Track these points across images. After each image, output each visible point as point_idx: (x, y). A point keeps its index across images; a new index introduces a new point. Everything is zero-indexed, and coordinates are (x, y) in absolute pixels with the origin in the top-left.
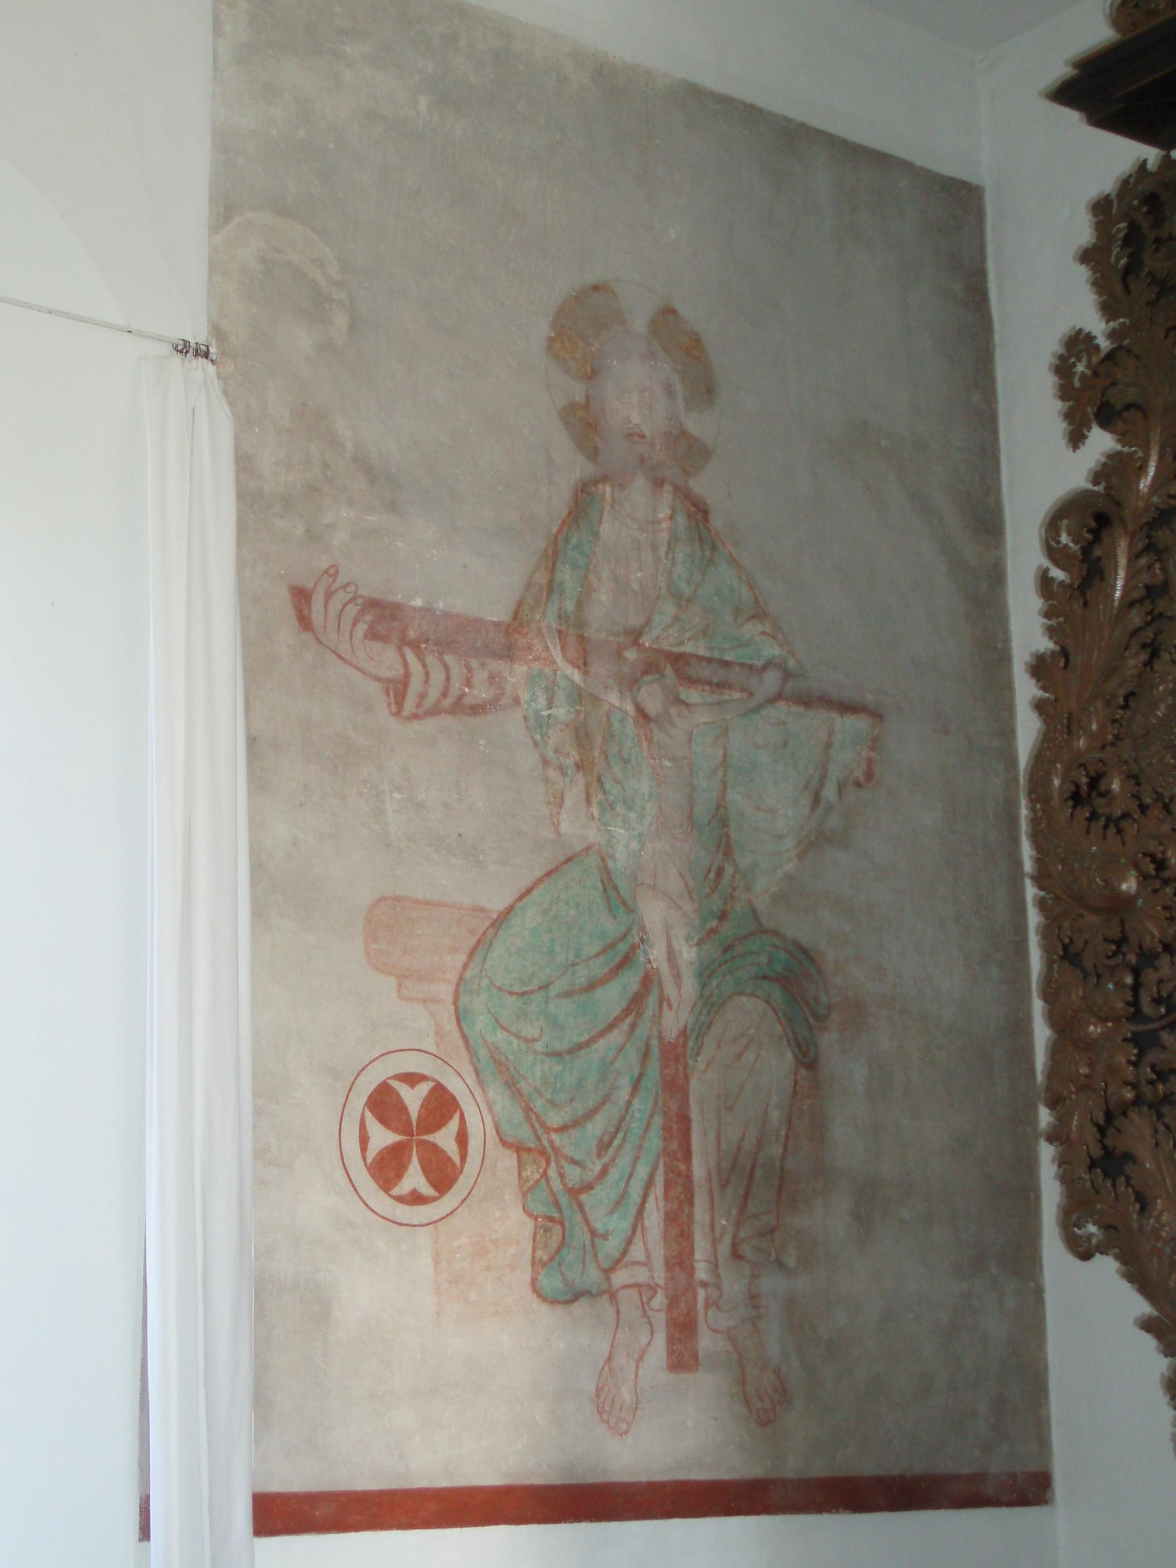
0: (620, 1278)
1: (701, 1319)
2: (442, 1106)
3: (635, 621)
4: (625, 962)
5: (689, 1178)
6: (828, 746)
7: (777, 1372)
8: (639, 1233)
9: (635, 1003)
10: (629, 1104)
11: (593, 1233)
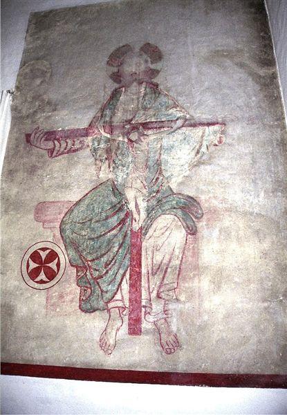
0: (111, 305)
1: (143, 319)
2: (53, 255)
3: (129, 117)
4: (120, 209)
5: (140, 273)
6: (202, 137)
7: (175, 336)
8: (119, 290)
9: (123, 222)
10: (118, 251)
11: (102, 291)
